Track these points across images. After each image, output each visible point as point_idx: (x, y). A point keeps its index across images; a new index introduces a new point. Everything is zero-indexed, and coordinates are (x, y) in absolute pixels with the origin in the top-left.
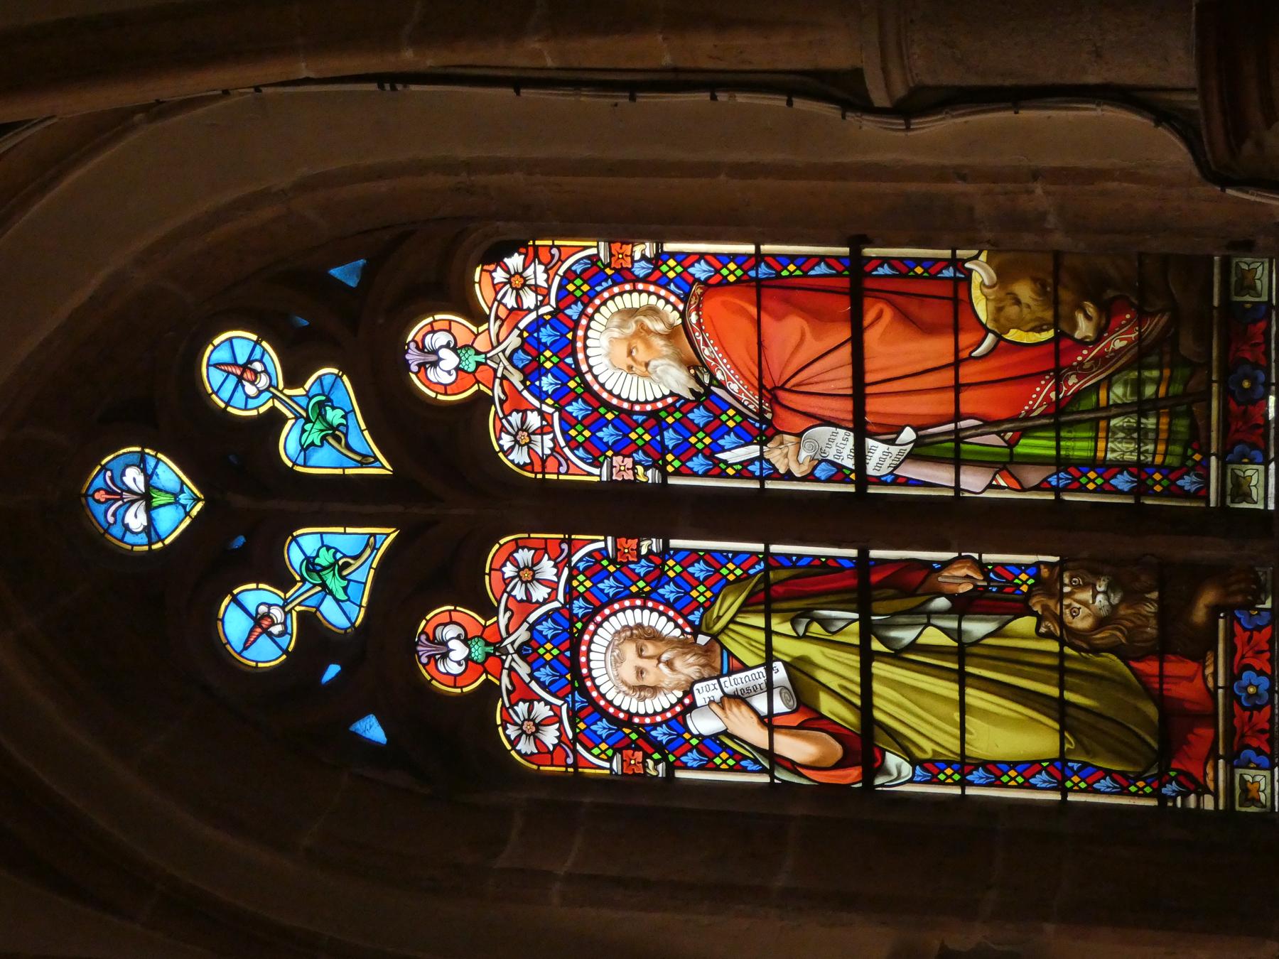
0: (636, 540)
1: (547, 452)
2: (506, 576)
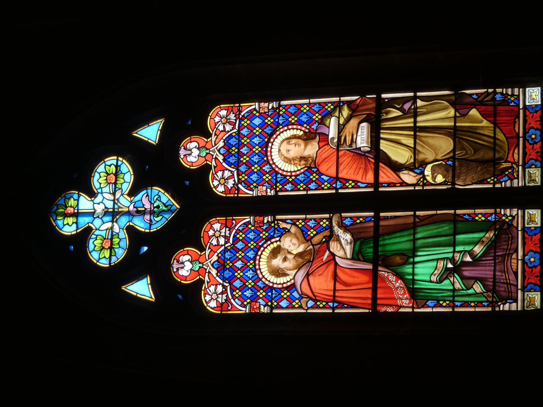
0: (263, 217)
1: (224, 301)
2: (210, 235)
